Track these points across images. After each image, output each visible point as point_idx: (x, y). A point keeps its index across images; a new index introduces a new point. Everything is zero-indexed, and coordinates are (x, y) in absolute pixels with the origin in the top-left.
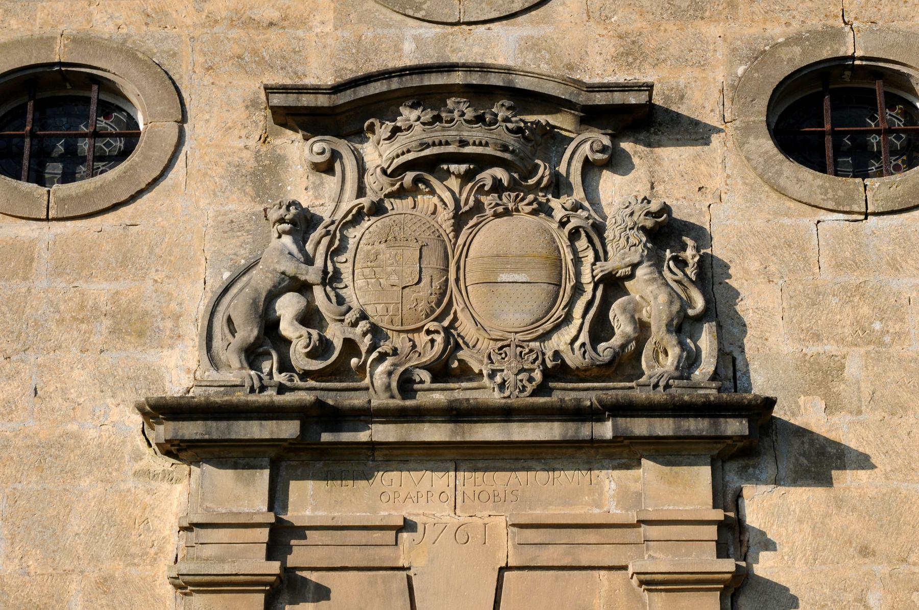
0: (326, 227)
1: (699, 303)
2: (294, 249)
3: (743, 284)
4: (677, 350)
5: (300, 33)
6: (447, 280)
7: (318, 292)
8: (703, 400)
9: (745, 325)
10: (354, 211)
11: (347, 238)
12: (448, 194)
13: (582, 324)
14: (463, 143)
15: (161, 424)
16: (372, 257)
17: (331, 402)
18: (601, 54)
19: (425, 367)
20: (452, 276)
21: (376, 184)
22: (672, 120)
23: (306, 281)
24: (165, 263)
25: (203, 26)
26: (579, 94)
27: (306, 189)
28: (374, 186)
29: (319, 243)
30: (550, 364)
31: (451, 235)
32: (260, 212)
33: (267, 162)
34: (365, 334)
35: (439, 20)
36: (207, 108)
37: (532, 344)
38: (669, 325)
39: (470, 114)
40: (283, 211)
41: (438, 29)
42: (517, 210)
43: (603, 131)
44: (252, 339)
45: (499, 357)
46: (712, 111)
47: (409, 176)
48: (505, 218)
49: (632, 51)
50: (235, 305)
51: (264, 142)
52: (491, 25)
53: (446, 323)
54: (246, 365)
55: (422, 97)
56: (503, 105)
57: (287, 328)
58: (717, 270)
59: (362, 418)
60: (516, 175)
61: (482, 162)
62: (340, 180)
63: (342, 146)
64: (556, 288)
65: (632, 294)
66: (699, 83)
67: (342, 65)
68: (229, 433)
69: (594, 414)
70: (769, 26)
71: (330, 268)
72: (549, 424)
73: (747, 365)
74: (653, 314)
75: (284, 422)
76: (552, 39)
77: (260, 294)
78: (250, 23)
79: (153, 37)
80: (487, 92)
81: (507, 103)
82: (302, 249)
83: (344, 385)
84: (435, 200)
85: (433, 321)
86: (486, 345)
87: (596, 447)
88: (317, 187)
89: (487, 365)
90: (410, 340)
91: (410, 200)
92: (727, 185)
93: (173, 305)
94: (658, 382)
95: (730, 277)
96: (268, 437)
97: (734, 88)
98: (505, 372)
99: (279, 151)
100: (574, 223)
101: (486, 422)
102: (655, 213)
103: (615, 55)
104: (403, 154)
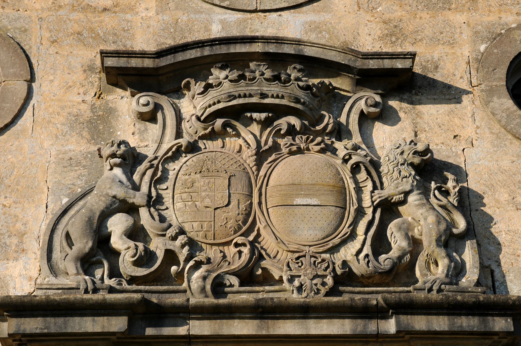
0: (150, 162)
1: (461, 224)
2: (124, 178)
3: (495, 211)
4: (446, 261)
5: (128, 17)
6: (251, 203)
7: (144, 212)
8: (474, 300)
9: (499, 244)
10: (174, 149)
11: (168, 170)
12: (251, 136)
13: (365, 239)
14: (264, 96)
15: (6, 321)
16: (189, 185)
17: (155, 301)
18: (370, 35)
19: (234, 273)
20: (255, 200)
21: (191, 129)
22: (429, 85)
23: (133, 203)
24: (13, 191)
25: (50, 9)
26: (355, 61)
27: (133, 134)
28: (190, 131)
29: (144, 174)
30: (339, 271)
31: (254, 169)
32: (94, 151)
33: (101, 113)
34: (183, 246)
35: (240, 8)
36: (52, 71)
37: (324, 256)
38: (438, 240)
39: (268, 74)
40: (115, 148)
41: (240, 15)
42: (308, 149)
43: (375, 91)
44: (87, 250)
45: (297, 266)
46: (461, 78)
47: (219, 122)
48: (298, 155)
49: (394, 31)
50: (73, 222)
51: (99, 98)
52: (282, 13)
53: (251, 238)
54: (81, 271)
55: (227, 62)
56: (295, 68)
57: (117, 241)
58: (473, 200)
59: (181, 315)
60: (306, 122)
62: (162, 126)
63: (164, 101)
64: (342, 210)
65: (405, 217)
66: (449, 56)
67: (162, 40)
68: (66, 328)
69: (379, 313)
70: (503, 15)
71: (154, 194)
72: (341, 321)
73: (504, 277)
74: (424, 232)
75: (114, 318)
76: (331, 23)
77: (94, 214)
78: (88, 8)
79: (8, 17)
80: (280, 59)
81: (298, 66)
82: (130, 178)
83: (165, 288)
84: (240, 141)
85: (241, 235)
86: (284, 256)
87: (381, 342)
88: (142, 132)
89: (286, 271)
90: (221, 252)
91: (219, 142)
92: (477, 133)
93: (19, 225)
94: (432, 286)
95: (484, 205)
96: (100, 330)
97: (478, 61)
98: (302, 277)
99: (110, 105)
100: (355, 159)
101: (288, 318)
102: (421, 152)
103: (381, 35)
104: (214, 104)
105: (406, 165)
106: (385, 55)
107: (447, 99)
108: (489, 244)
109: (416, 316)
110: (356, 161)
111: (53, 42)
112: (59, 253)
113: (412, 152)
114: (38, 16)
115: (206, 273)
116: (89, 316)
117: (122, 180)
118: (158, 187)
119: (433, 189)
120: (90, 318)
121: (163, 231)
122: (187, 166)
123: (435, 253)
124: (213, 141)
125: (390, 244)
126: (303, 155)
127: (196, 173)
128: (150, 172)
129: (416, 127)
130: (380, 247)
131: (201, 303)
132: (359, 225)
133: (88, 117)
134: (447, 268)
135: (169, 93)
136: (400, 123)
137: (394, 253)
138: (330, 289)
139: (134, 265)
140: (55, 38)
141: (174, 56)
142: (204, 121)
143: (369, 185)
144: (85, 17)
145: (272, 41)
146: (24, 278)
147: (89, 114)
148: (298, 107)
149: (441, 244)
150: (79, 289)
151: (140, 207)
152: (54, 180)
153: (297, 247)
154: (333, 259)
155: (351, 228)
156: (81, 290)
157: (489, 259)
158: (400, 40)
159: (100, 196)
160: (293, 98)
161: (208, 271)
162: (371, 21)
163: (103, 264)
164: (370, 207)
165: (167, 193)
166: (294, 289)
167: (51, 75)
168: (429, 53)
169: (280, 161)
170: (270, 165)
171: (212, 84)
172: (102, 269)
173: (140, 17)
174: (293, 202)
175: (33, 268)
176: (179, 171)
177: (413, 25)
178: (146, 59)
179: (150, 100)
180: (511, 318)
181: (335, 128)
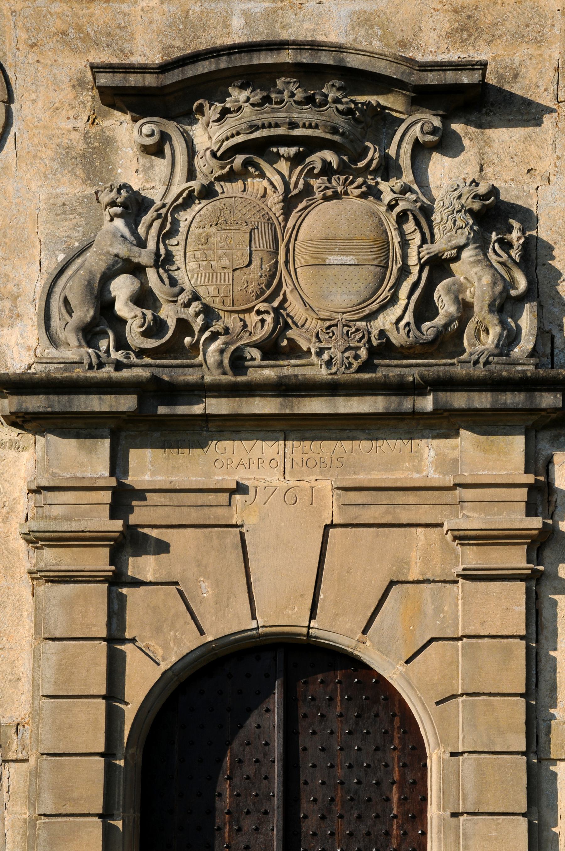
1: (522, 283)
2: (126, 232)
4: (498, 329)
6: (277, 262)
7: (151, 274)
8: (520, 375)
10: (185, 195)
13: (407, 305)
14: (293, 125)
16: (203, 240)
17: (166, 378)
19: (255, 345)
23: (139, 263)
26: (410, 74)
27: (137, 172)
29: (150, 226)
30: (375, 342)
31: (281, 219)
33: (96, 144)
34: (197, 314)
36: (34, 88)
37: (359, 324)
38: (491, 306)
39: (299, 95)
40: (114, 194)
42: (346, 193)
43: (434, 112)
44: (88, 319)
45: (327, 336)
46: (546, 90)
47: (239, 159)
48: (334, 201)
50: (71, 286)
53: (276, 304)
54: (84, 343)
55: (253, 77)
56: (333, 85)
57: (122, 308)
58: (542, 252)
59: (196, 392)
60: (345, 158)
61: (312, 145)
62: (170, 162)
63: (172, 128)
65: (457, 276)
66: (534, 61)
68: (71, 406)
69: (417, 389)
71: (162, 251)
72: (373, 398)
74: (476, 295)
75: (122, 396)
76: (385, 14)
77: (94, 276)
81: (338, 83)
82: (134, 232)
84: (265, 183)
85: (263, 301)
86: (314, 325)
88: (148, 169)
89: (315, 343)
90: (241, 320)
92: (556, 166)
93: (10, 286)
95: (553, 258)
96: (107, 410)
98: (332, 350)
99: (108, 133)
100: (402, 206)
101: (314, 396)
102: (483, 196)
103: (449, 31)
104: (233, 136)
105: (463, 212)
106: (447, 66)
107: (524, 120)
108: (553, 305)
109: (456, 393)
110: (403, 208)
111: (32, 46)
112: (58, 321)
113: (472, 195)
114: (10, 8)
115: (224, 346)
116: (95, 394)
117: (124, 234)
118: (167, 242)
119: (493, 240)
120: (96, 396)
121: (174, 297)
122: (201, 216)
123: (486, 321)
124: (232, 182)
125: (438, 308)
126: (340, 201)
127: (211, 226)
128: (157, 224)
129: (483, 159)
130: (426, 312)
131: (217, 381)
132: (402, 287)
133: (81, 150)
134: (498, 337)
135: (179, 117)
136: (463, 153)
137: (439, 320)
138: (363, 363)
139: (142, 336)
140: (34, 41)
141: (182, 70)
142: (221, 158)
143: (417, 238)
144: (70, 9)
145: (306, 47)
146: (21, 347)
147: (81, 146)
148: (335, 139)
149: (494, 309)
150: (83, 363)
151: (147, 267)
152: (47, 231)
153: (328, 314)
154: (369, 328)
155: (391, 292)
156: (84, 364)
157: (551, 323)
158: (473, 37)
159: (100, 254)
160: (329, 128)
161: (226, 343)
162: (438, 10)
163: (108, 334)
164: (417, 265)
165: (178, 250)
166: (323, 363)
167: (33, 92)
168: (509, 55)
169: (312, 209)
170: (300, 214)
171: (230, 109)
172: (107, 340)
173: (140, 8)
174: (325, 261)
175: (31, 336)
176: (192, 222)
177: (492, 15)
178: (148, 76)
179: (155, 129)
180: (561, 393)
181: (381, 165)
